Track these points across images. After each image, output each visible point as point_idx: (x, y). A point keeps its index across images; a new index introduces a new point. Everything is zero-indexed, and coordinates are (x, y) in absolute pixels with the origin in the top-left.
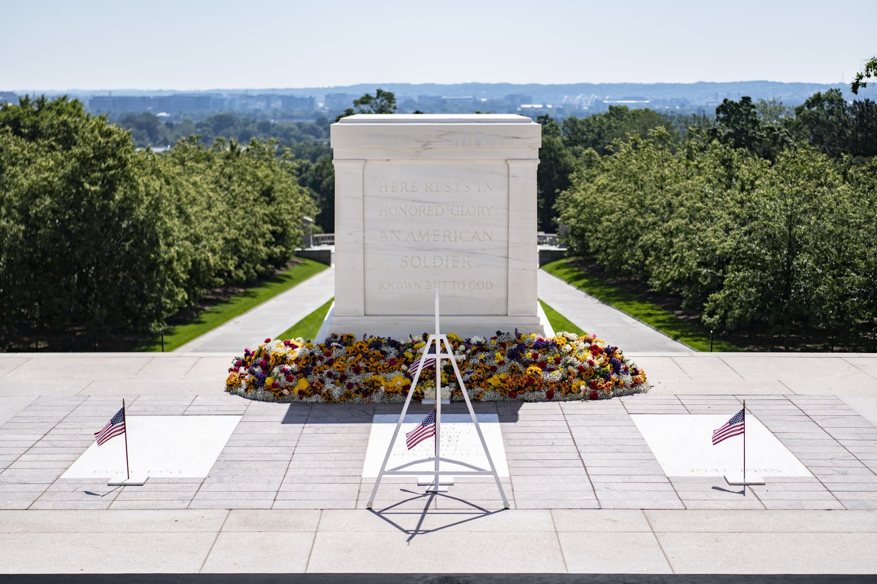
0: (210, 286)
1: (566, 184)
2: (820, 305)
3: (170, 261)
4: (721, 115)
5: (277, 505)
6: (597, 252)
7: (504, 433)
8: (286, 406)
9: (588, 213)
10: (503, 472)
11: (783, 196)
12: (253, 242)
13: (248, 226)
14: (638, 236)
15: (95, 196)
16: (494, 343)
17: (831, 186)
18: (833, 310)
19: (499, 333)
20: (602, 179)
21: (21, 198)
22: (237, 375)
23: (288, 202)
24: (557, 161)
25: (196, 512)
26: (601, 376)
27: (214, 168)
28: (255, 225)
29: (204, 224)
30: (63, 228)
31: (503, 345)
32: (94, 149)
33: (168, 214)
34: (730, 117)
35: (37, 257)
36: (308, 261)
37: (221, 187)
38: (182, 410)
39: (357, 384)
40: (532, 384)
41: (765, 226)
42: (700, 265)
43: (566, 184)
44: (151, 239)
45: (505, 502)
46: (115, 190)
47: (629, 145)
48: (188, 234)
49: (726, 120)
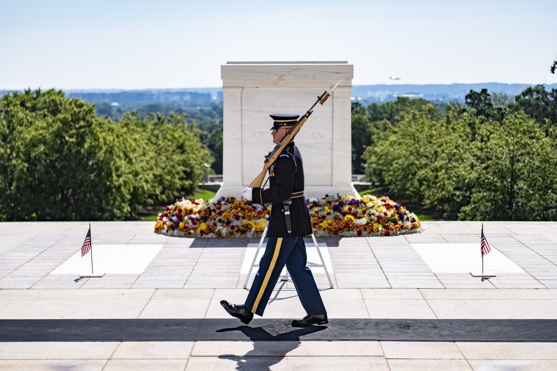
0: (145, 205)
1: (370, 143)
2: (532, 214)
3: (120, 187)
4: (469, 101)
5: (186, 286)
6: (390, 184)
7: (330, 252)
8: (192, 240)
9: (384, 159)
10: (330, 271)
11: (507, 144)
12: (172, 178)
13: (169, 167)
14: (415, 173)
15: (72, 145)
16: (324, 201)
17: (538, 139)
18: (540, 217)
19: (327, 196)
20: (393, 138)
21: (26, 146)
22: (161, 222)
23: (194, 153)
24: (364, 131)
25: (135, 290)
26: (392, 222)
27: (147, 131)
28: (173, 167)
29: (141, 165)
30: (52, 165)
31: (329, 203)
32: (71, 115)
33: (119, 157)
34: (474, 101)
35: (36, 184)
36: (207, 192)
37: (152, 143)
38: (126, 242)
39: (237, 226)
40: (348, 226)
41: (497, 163)
42: (456, 189)
43: (370, 143)
44: (107, 172)
45: (331, 284)
46: (85, 141)
47: (411, 116)
48: (130, 170)
49: (472, 104)
